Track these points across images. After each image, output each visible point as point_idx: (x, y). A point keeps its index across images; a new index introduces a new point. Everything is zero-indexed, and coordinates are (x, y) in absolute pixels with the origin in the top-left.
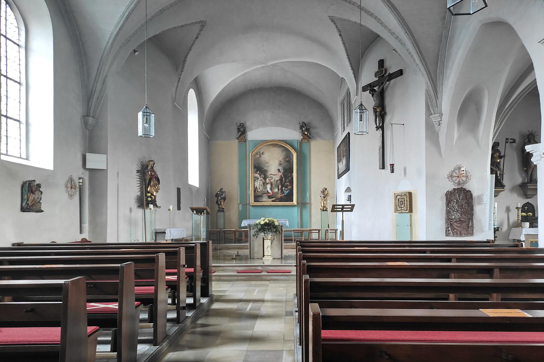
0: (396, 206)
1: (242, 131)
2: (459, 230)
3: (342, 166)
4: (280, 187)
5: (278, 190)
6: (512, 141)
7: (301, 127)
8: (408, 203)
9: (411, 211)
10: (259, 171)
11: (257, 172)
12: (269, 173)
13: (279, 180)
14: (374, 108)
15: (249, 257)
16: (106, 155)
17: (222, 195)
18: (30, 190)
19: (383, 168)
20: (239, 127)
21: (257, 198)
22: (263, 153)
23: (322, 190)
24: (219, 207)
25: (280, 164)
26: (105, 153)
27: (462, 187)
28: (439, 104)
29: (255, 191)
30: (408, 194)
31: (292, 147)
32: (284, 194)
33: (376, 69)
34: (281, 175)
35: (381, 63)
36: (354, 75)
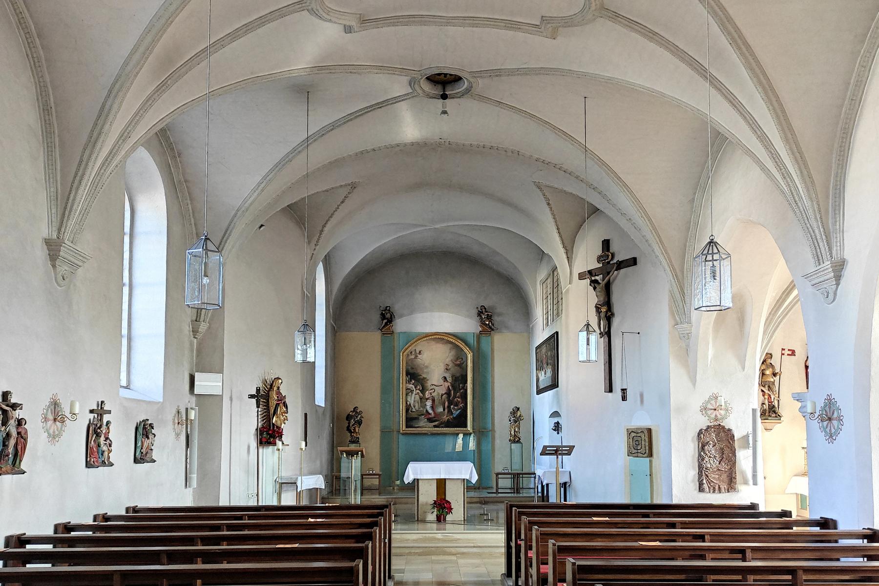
0: (629, 447)
1: (387, 318)
2: (717, 484)
3: (545, 377)
4: (447, 404)
5: (444, 410)
6: (790, 353)
7: (480, 314)
8: (647, 444)
9: (651, 455)
10: (415, 380)
11: (411, 381)
12: (429, 384)
13: (445, 394)
14: (596, 307)
15: (416, 519)
16: (221, 374)
17: (357, 417)
18: (145, 433)
19: (611, 391)
20: (384, 312)
21: (410, 421)
22: (420, 352)
23: (512, 410)
24: (351, 436)
25: (447, 369)
26: (221, 371)
27: (720, 423)
28: (687, 311)
29: (407, 410)
30: (646, 432)
31: (465, 344)
32: (452, 415)
33: (599, 251)
34: (449, 386)
35: (606, 244)
36: (567, 255)
